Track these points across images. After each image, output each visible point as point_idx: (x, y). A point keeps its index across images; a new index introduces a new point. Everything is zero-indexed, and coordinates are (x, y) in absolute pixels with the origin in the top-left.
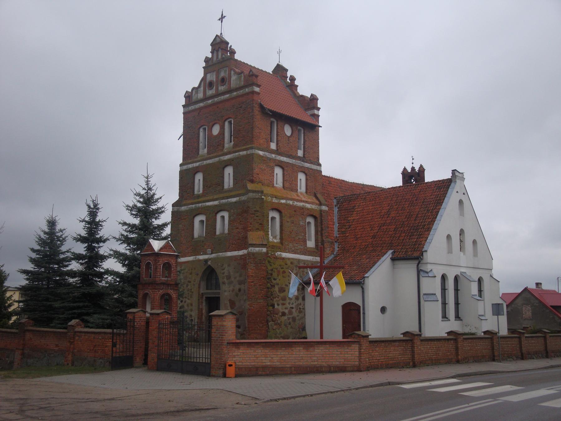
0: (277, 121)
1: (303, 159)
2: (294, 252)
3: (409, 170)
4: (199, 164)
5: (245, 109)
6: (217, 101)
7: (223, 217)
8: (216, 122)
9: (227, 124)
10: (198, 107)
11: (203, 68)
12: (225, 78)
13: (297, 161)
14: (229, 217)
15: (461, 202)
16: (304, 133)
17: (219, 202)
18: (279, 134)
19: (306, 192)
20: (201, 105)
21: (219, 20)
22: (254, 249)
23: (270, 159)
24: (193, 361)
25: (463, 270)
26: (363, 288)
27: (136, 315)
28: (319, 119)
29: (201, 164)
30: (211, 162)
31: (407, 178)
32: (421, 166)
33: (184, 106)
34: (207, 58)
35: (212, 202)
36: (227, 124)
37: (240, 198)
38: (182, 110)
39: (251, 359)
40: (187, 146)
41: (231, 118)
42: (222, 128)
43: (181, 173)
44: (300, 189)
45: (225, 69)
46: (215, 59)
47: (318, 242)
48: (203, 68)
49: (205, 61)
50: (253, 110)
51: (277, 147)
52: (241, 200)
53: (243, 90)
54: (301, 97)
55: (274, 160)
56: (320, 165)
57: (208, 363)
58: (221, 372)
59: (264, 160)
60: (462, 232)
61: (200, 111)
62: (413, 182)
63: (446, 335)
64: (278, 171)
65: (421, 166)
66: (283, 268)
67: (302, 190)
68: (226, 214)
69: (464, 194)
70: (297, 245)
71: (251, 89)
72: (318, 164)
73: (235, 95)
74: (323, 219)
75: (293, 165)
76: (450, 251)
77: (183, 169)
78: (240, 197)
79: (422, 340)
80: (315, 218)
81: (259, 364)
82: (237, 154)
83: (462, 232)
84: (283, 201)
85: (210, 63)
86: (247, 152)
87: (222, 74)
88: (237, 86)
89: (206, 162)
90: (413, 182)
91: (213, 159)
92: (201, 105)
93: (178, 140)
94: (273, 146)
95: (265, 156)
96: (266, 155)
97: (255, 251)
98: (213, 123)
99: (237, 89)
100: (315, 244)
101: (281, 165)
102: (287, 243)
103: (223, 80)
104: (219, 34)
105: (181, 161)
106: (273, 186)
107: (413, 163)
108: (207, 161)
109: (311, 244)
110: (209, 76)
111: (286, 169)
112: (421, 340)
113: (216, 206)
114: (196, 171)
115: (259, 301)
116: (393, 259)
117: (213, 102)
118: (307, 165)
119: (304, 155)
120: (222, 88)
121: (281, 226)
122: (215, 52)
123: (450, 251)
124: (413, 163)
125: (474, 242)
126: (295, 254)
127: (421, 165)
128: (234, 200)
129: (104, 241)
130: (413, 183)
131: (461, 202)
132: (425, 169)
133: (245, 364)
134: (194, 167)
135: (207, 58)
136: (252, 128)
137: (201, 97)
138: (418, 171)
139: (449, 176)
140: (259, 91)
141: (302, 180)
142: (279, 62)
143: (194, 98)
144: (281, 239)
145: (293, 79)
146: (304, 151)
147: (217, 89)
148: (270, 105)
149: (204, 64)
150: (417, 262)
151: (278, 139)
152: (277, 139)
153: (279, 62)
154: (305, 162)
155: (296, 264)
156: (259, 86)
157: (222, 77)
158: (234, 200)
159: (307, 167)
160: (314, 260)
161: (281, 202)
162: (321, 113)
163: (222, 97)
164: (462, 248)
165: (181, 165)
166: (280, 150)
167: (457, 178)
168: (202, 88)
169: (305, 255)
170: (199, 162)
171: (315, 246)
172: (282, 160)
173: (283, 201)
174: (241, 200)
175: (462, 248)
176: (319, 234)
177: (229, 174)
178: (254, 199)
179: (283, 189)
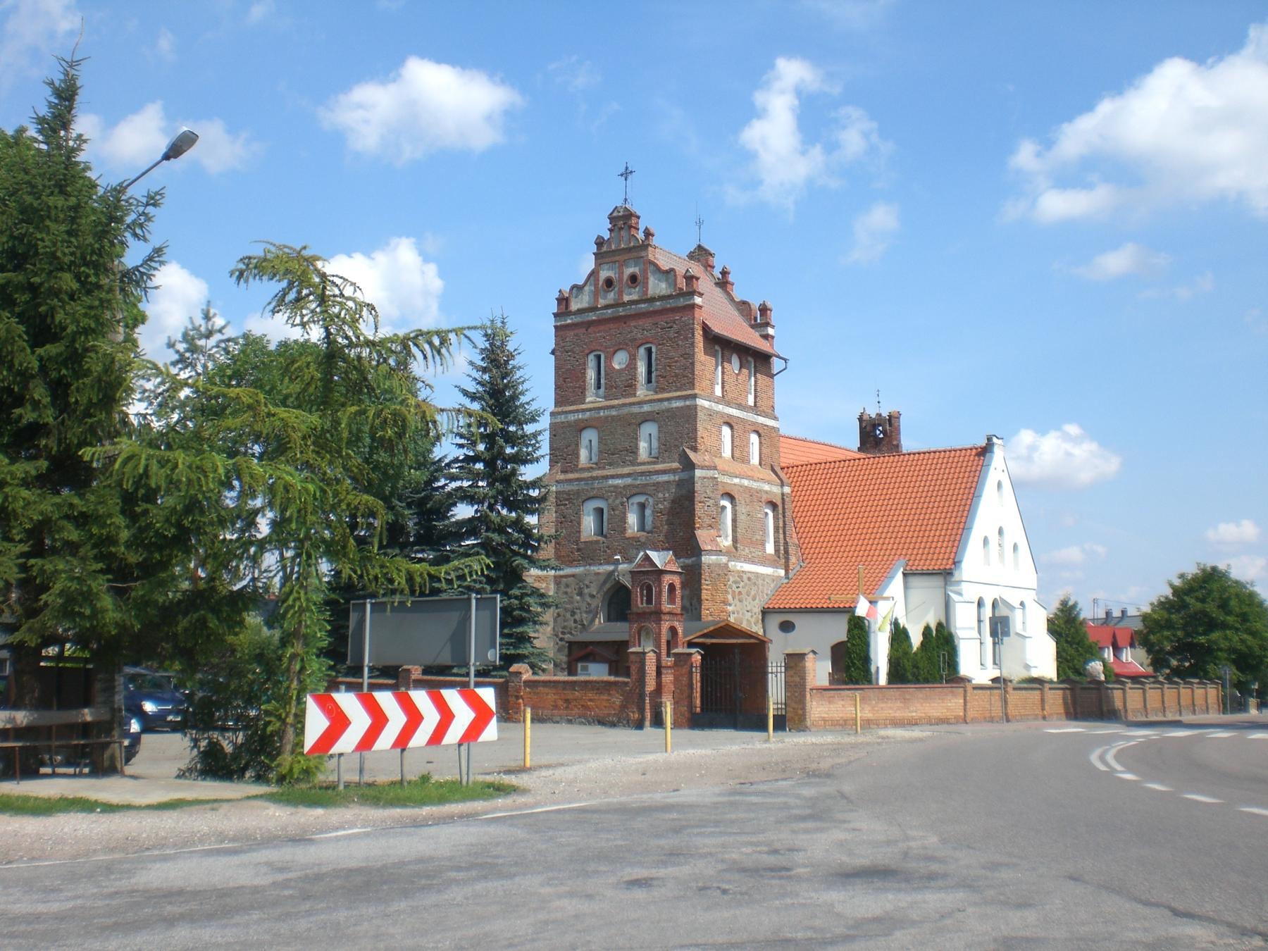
0: (722, 350)
1: (755, 409)
16: (755, 367)
19: (760, 464)
21: (622, 175)
23: (718, 413)
33: (556, 315)
34: (599, 237)
36: (642, 351)
38: (551, 322)
41: (651, 343)
42: (633, 358)
50: (693, 335)
51: (723, 392)
55: (722, 415)
60: (1001, 532)
63: (990, 682)
80: (774, 506)
84: (736, 481)
85: (605, 249)
94: (718, 391)
98: (616, 348)
102: (742, 548)
106: (721, 457)
109: (770, 548)
111: (736, 427)
114: (580, 427)
116: (904, 574)
117: (614, 315)
118: (761, 420)
119: (755, 402)
121: (734, 521)
140: (701, 304)
144: (735, 540)
146: (756, 397)
148: (718, 328)
152: (723, 378)
156: (701, 295)
160: (776, 574)
164: (1001, 555)
173: (736, 481)
175: (1001, 555)
176: (781, 531)
177: (650, 435)
178: (705, 478)
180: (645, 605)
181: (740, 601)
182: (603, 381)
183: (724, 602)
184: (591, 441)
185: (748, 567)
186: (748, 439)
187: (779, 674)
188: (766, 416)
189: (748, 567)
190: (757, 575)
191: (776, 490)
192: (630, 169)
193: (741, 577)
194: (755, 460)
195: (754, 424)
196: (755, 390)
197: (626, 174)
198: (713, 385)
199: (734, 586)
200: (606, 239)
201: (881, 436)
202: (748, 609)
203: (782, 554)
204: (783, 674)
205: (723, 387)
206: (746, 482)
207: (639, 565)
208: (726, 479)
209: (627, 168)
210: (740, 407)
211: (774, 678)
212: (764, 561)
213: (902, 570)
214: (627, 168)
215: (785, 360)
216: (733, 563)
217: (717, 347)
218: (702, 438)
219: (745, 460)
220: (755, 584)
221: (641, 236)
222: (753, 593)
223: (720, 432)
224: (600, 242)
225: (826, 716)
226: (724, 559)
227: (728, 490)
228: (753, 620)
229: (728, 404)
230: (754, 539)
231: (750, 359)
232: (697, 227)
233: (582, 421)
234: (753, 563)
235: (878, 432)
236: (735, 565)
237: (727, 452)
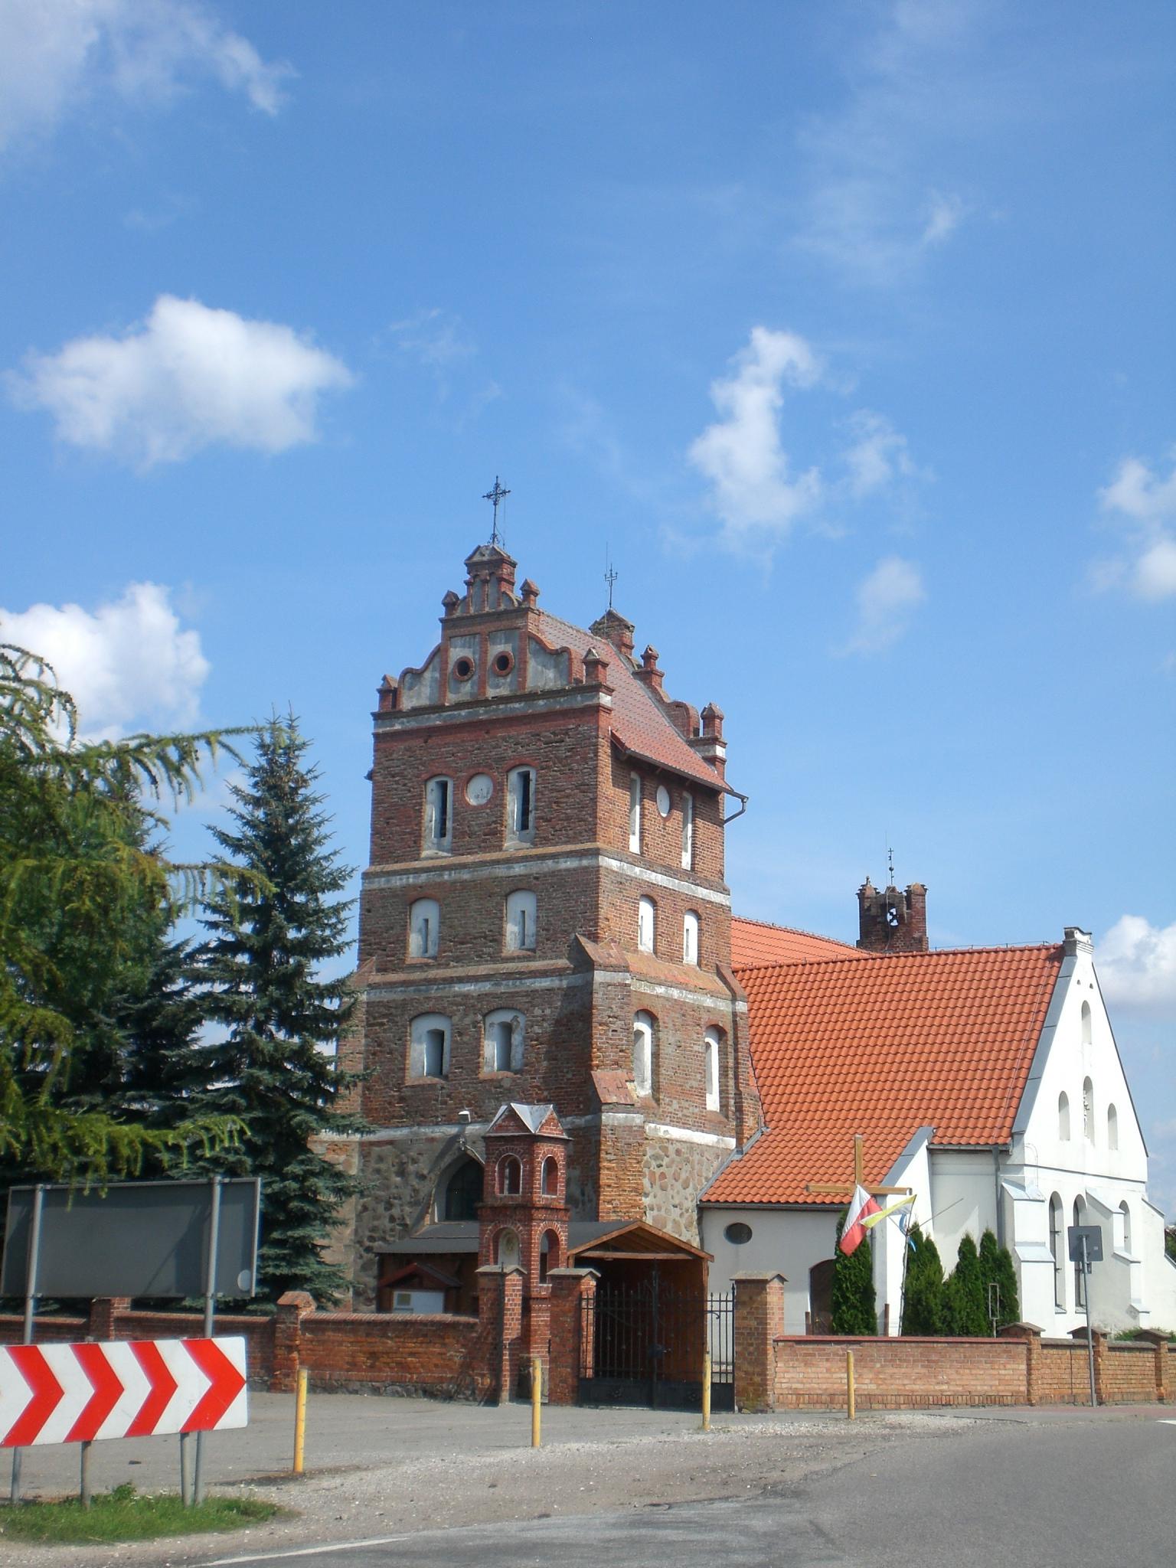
1: (693, 875)
2: (683, 1123)
8: (480, 770)
11: (441, 620)
18: (646, 812)
19: (699, 964)
21: (489, 496)
23: (632, 879)
27: (509, 1280)
33: (377, 717)
34: (450, 594)
39: (820, 1376)
42: (499, 789)
44: (687, 955)
47: (728, 1098)
48: (441, 620)
51: (641, 847)
55: (639, 883)
57: (727, 1384)
59: (622, 881)
60: (1088, 1085)
62: (891, 921)
63: (1070, 1337)
66: (662, 1166)
67: (689, 959)
69: (1091, 986)
70: (686, 1105)
72: (724, 889)
74: (739, 1035)
75: (672, 893)
76: (1065, 1135)
79: (1045, 1346)
80: (719, 1032)
81: (836, 1386)
83: (1088, 1085)
84: (660, 990)
85: (458, 613)
90: (891, 921)
94: (634, 845)
98: (472, 771)
100: (720, 1102)
106: (636, 951)
109: (713, 1102)
111: (661, 903)
112: (1042, 1345)
114: (411, 898)
116: (931, 1152)
118: (702, 892)
119: (693, 864)
121: (656, 1055)
123: (1065, 1135)
126: (684, 1128)
130: (892, 924)
133: (808, 1386)
135: (450, 594)
136: (594, 800)
140: (609, 705)
144: (656, 1088)
146: (694, 856)
148: (635, 745)
149: (441, 612)
151: (643, 825)
152: (642, 825)
155: (686, 1156)
160: (722, 1146)
167: (1079, 946)
169: (703, 1131)
172: (654, 882)
173: (660, 990)
176: (731, 1074)
177: (523, 912)
180: (506, 1193)
181: (663, 1189)
182: (449, 824)
183: (635, 1190)
184: (427, 921)
185: (676, 1133)
187: (723, 1314)
188: (710, 887)
189: (676, 1133)
190: (692, 1146)
191: (724, 1006)
192: (502, 487)
193: (665, 1149)
194: (691, 956)
196: (694, 845)
197: (497, 494)
199: (654, 1164)
202: (676, 1202)
203: (733, 1114)
204: (730, 1314)
205: (642, 839)
206: (675, 993)
207: (500, 1127)
208: (644, 988)
209: (497, 486)
210: (670, 871)
212: (703, 1123)
213: (926, 1143)
214: (497, 486)
215: (743, 798)
216: (652, 1125)
218: (607, 919)
220: (687, 1161)
222: (683, 1176)
223: (636, 910)
225: (799, 1386)
226: (638, 1119)
227: (646, 1004)
228: (683, 1221)
229: (650, 866)
233: (415, 887)
234: (685, 1125)
235: (889, 917)
236: (656, 1129)
237: (646, 942)
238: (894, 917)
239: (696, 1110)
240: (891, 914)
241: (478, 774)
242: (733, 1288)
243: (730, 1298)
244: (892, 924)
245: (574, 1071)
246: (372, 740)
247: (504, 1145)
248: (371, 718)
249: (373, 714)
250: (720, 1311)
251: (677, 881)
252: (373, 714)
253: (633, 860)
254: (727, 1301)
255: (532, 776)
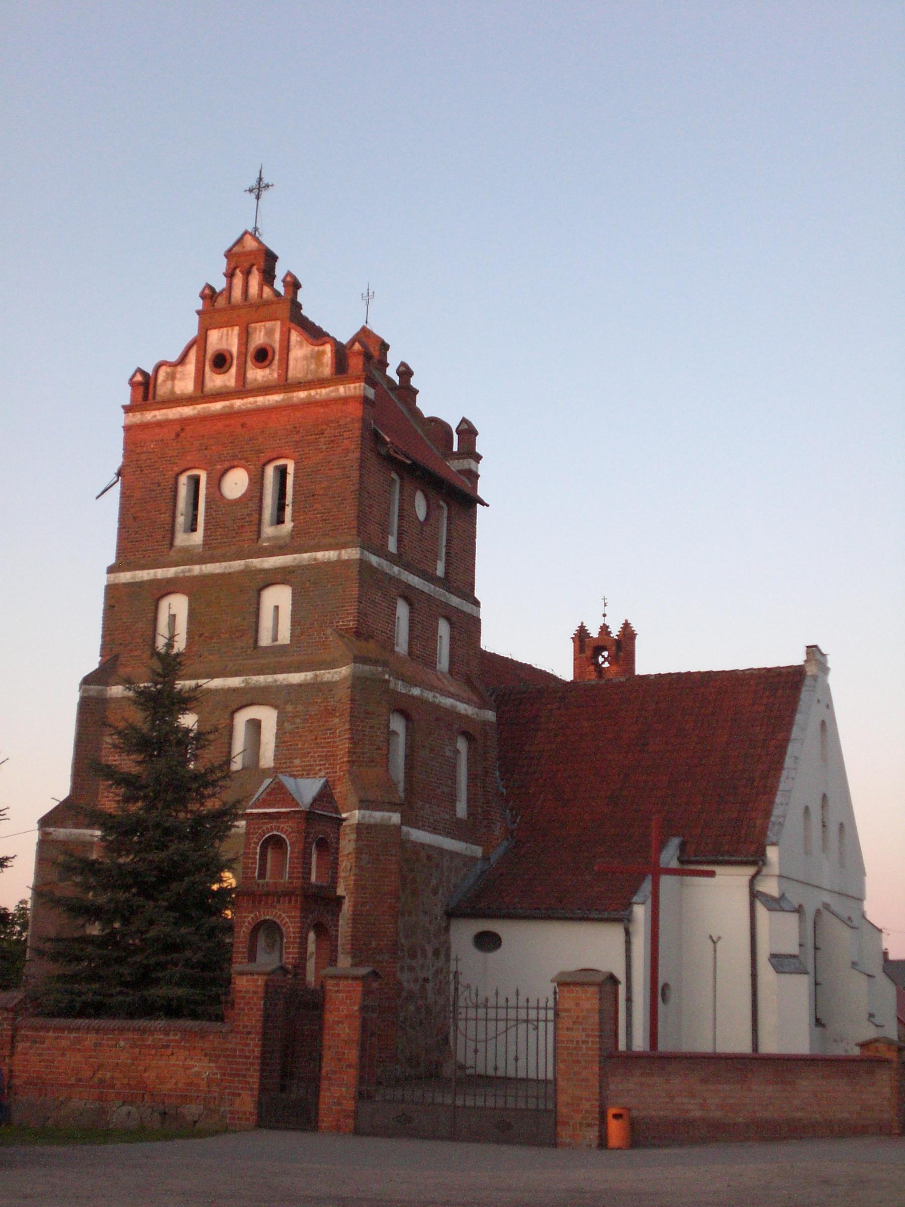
0: (401, 478)
1: (445, 582)
3: (594, 632)
4: (176, 573)
5: (332, 441)
6: (242, 407)
7: (255, 725)
9: (270, 471)
10: (177, 416)
11: (199, 312)
12: (269, 349)
13: (438, 589)
14: (280, 724)
15: (823, 724)
16: (449, 518)
17: (246, 681)
20: (188, 411)
21: (251, 191)
22: (370, 816)
23: (391, 578)
24: (524, 1107)
25: (827, 898)
26: (627, 933)
28: (477, 482)
29: (183, 572)
30: (218, 571)
31: (589, 652)
32: (626, 625)
33: (128, 409)
35: (221, 679)
37: (316, 676)
38: (121, 419)
40: (135, 518)
43: (111, 591)
45: (269, 324)
46: (237, 293)
48: (199, 312)
49: (203, 296)
51: (398, 548)
52: (319, 679)
53: (328, 389)
54: (432, 421)
56: (477, 603)
58: (592, 1134)
61: (182, 430)
62: (603, 663)
64: (402, 610)
65: (626, 625)
67: (442, 665)
68: (268, 717)
71: (355, 388)
73: (302, 399)
75: (429, 598)
77: (117, 582)
78: (318, 672)
80: (469, 737)
82: (306, 556)
86: (339, 555)
87: (259, 338)
88: (310, 377)
89: (201, 570)
90: (603, 663)
91: (224, 564)
92: (188, 411)
93: (97, 497)
94: (392, 546)
95: (380, 568)
96: (382, 567)
97: (372, 821)
99: (300, 385)
101: (410, 595)
103: (262, 356)
104: (250, 230)
105: (111, 560)
106: (392, 650)
107: (604, 615)
108: (203, 567)
109: (461, 810)
110: (214, 336)
113: (235, 690)
115: (379, 958)
118: (455, 601)
119: (446, 573)
120: (257, 375)
122: (239, 273)
124: (604, 615)
125: (841, 825)
127: (626, 621)
128: (296, 678)
129: (231, 780)
130: (603, 666)
131: (823, 724)
132: (636, 634)
134: (158, 580)
135: (209, 287)
137: (185, 392)
138: (617, 635)
139: (797, 658)
141: (443, 638)
142: (367, 322)
143: (163, 389)
145: (405, 372)
146: (448, 564)
147: (242, 375)
149: (199, 304)
150: (751, 870)
152: (399, 526)
153: (367, 322)
154: (452, 593)
157: (255, 348)
158: (296, 678)
159: (454, 605)
160: (468, 853)
161: (413, 694)
162: (482, 468)
163: (261, 400)
165: (111, 570)
166: (406, 557)
168: (190, 368)
170: (175, 566)
171: (466, 816)
173: (416, 691)
174: (319, 679)
179: (409, 658)
186: (435, 631)
187: (542, 1025)
190: (441, 851)
194: (444, 663)
195: (447, 605)
196: (448, 554)
197: (259, 188)
198: (385, 533)
200: (218, 290)
201: (606, 665)
204: (551, 1026)
209: (258, 198)
210: (430, 577)
211: (532, 1034)
212: (457, 830)
214: (258, 198)
217: (394, 476)
219: (430, 661)
220: (437, 866)
221: (279, 286)
222: (434, 882)
223: (394, 609)
224: (209, 295)
229: (408, 567)
230: (439, 791)
231: (442, 503)
232: (364, 302)
234: (435, 830)
235: (601, 660)
237: (402, 645)
238: (606, 659)
239: (447, 817)
240: (603, 656)
241: (233, 467)
242: (555, 993)
243: (551, 1004)
244: (603, 666)
245: (328, 768)
246: (121, 434)
247: (269, 823)
248: (122, 411)
249: (124, 407)
250: (538, 1020)
251: (433, 586)
252: (124, 407)
253: (395, 559)
254: (546, 1008)
255: (291, 469)
